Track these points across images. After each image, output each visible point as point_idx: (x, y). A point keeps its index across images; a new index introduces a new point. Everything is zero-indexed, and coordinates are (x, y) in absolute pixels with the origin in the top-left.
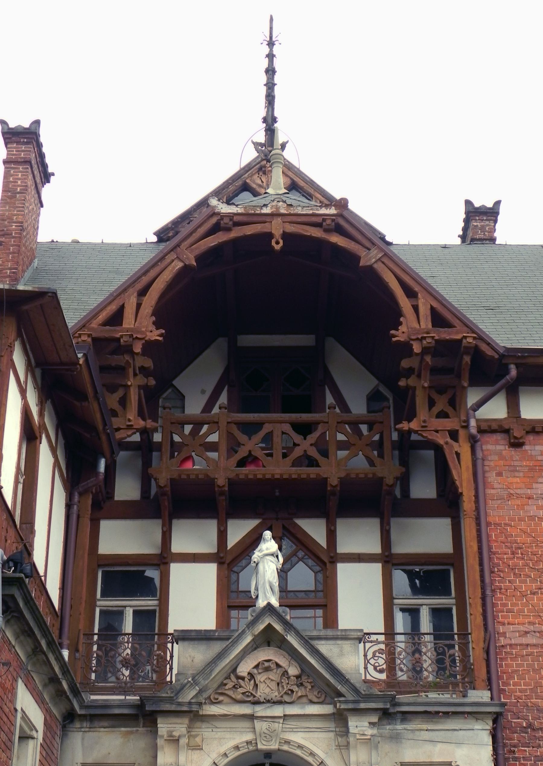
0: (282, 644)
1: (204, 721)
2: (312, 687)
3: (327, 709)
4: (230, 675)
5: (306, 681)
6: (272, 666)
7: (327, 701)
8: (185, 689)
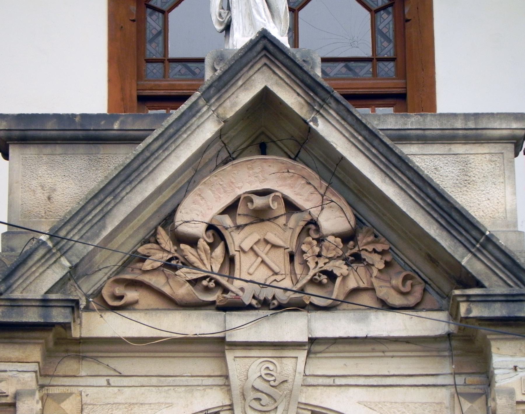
0: (303, 146)
1: (84, 358)
2: (388, 264)
3: (429, 324)
4: (155, 234)
5: (370, 248)
6: (274, 206)
7: (427, 303)
8: (30, 263)
